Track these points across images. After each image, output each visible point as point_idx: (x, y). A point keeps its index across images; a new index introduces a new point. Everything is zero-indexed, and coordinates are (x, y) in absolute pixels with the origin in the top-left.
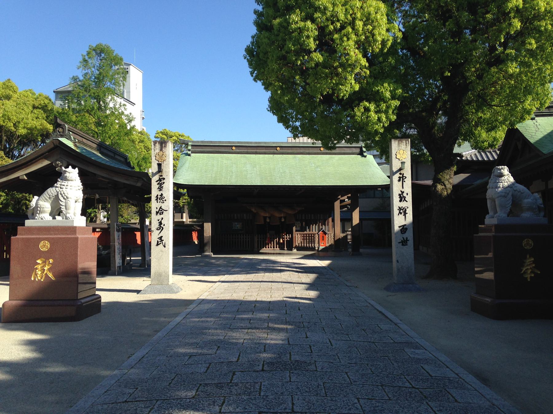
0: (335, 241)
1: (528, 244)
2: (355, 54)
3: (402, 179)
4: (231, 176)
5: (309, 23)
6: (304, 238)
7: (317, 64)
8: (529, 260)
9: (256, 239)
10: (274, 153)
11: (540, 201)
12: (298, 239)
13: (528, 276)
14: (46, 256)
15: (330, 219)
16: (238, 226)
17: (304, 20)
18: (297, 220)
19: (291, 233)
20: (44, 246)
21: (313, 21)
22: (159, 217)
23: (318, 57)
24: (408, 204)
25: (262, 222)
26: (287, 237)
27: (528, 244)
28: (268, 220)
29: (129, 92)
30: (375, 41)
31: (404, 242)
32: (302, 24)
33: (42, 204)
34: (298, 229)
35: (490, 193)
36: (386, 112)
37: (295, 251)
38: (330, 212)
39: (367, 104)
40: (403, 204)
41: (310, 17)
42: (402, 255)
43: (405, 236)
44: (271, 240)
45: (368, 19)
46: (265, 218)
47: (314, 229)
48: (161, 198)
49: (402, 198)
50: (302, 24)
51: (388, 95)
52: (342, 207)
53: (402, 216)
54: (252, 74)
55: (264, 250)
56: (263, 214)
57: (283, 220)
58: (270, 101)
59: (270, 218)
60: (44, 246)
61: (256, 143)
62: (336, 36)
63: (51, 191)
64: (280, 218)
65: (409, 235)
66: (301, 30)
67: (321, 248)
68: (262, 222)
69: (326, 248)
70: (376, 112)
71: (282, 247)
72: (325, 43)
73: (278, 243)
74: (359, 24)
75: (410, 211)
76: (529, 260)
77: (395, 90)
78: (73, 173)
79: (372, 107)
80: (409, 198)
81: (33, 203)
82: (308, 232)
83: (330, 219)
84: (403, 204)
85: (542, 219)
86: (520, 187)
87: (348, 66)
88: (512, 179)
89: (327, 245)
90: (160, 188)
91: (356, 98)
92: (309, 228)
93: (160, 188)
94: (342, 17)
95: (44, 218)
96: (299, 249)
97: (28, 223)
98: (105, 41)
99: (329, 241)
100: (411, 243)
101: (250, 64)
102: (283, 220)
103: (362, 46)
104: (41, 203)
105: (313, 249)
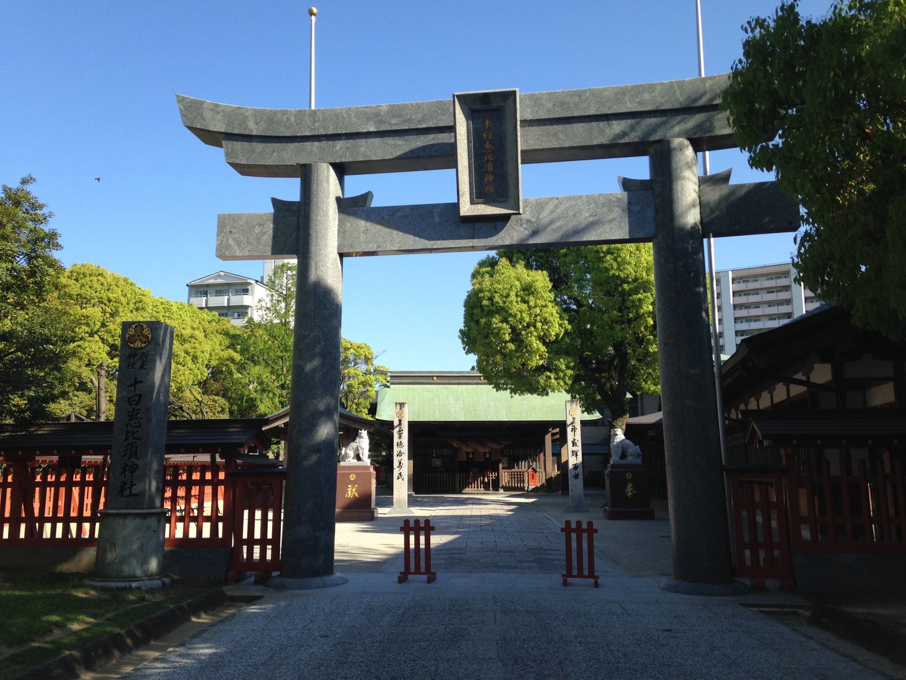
0: (547, 480)
1: (629, 476)
2: (537, 344)
4: (434, 411)
5: (505, 324)
6: (512, 476)
7: (511, 351)
8: (630, 485)
9: (458, 479)
10: (478, 384)
11: (639, 450)
12: (505, 477)
13: (629, 495)
14: (353, 483)
15: (542, 454)
16: (437, 462)
17: (502, 322)
20: (353, 477)
21: (507, 322)
22: (399, 458)
23: (512, 346)
24: (579, 449)
25: (465, 458)
26: (493, 476)
27: (629, 476)
28: (471, 456)
30: (550, 335)
31: (576, 476)
32: (500, 325)
33: (349, 451)
34: (505, 466)
35: (611, 446)
36: (564, 378)
37: (502, 491)
38: (541, 447)
39: (548, 374)
40: (575, 449)
41: (505, 320)
42: (576, 486)
43: (577, 472)
44: (475, 479)
45: (545, 322)
46: (468, 453)
47: (523, 466)
48: (400, 444)
49: (574, 444)
50: (500, 325)
51: (563, 367)
52: (553, 441)
53: (574, 457)
54: (464, 348)
55: (467, 490)
57: (488, 456)
58: (465, 306)
59: (473, 453)
60: (353, 477)
61: (459, 372)
62: (523, 332)
63: (353, 445)
64: (485, 454)
65: (580, 471)
66: (500, 329)
67: (531, 487)
68: (465, 458)
69: (537, 487)
70: (555, 379)
71: (486, 487)
72: (516, 337)
73: (483, 482)
74: (539, 325)
75: (580, 454)
76: (630, 485)
77: (569, 363)
78: (364, 433)
79: (552, 376)
80: (579, 444)
81: (343, 452)
82: (516, 469)
83: (542, 454)
84: (575, 449)
85: (639, 461)
86: (628, 441)
87: (531, 352)
88: (623, 437)
89: (539, 485)
90: (400, 437)
91: (540, 369)
92: (518, 465)
93: (400, 437)
94: (527, 319)
95: (351, 461)
96: (506, 489)
97: (342, 464)
99: (539, 480)
100: (581, 477)
101: (463, 342)
102: (488, 456)
103: (542, 339)
104: (348, 452)
105: (522, 489)
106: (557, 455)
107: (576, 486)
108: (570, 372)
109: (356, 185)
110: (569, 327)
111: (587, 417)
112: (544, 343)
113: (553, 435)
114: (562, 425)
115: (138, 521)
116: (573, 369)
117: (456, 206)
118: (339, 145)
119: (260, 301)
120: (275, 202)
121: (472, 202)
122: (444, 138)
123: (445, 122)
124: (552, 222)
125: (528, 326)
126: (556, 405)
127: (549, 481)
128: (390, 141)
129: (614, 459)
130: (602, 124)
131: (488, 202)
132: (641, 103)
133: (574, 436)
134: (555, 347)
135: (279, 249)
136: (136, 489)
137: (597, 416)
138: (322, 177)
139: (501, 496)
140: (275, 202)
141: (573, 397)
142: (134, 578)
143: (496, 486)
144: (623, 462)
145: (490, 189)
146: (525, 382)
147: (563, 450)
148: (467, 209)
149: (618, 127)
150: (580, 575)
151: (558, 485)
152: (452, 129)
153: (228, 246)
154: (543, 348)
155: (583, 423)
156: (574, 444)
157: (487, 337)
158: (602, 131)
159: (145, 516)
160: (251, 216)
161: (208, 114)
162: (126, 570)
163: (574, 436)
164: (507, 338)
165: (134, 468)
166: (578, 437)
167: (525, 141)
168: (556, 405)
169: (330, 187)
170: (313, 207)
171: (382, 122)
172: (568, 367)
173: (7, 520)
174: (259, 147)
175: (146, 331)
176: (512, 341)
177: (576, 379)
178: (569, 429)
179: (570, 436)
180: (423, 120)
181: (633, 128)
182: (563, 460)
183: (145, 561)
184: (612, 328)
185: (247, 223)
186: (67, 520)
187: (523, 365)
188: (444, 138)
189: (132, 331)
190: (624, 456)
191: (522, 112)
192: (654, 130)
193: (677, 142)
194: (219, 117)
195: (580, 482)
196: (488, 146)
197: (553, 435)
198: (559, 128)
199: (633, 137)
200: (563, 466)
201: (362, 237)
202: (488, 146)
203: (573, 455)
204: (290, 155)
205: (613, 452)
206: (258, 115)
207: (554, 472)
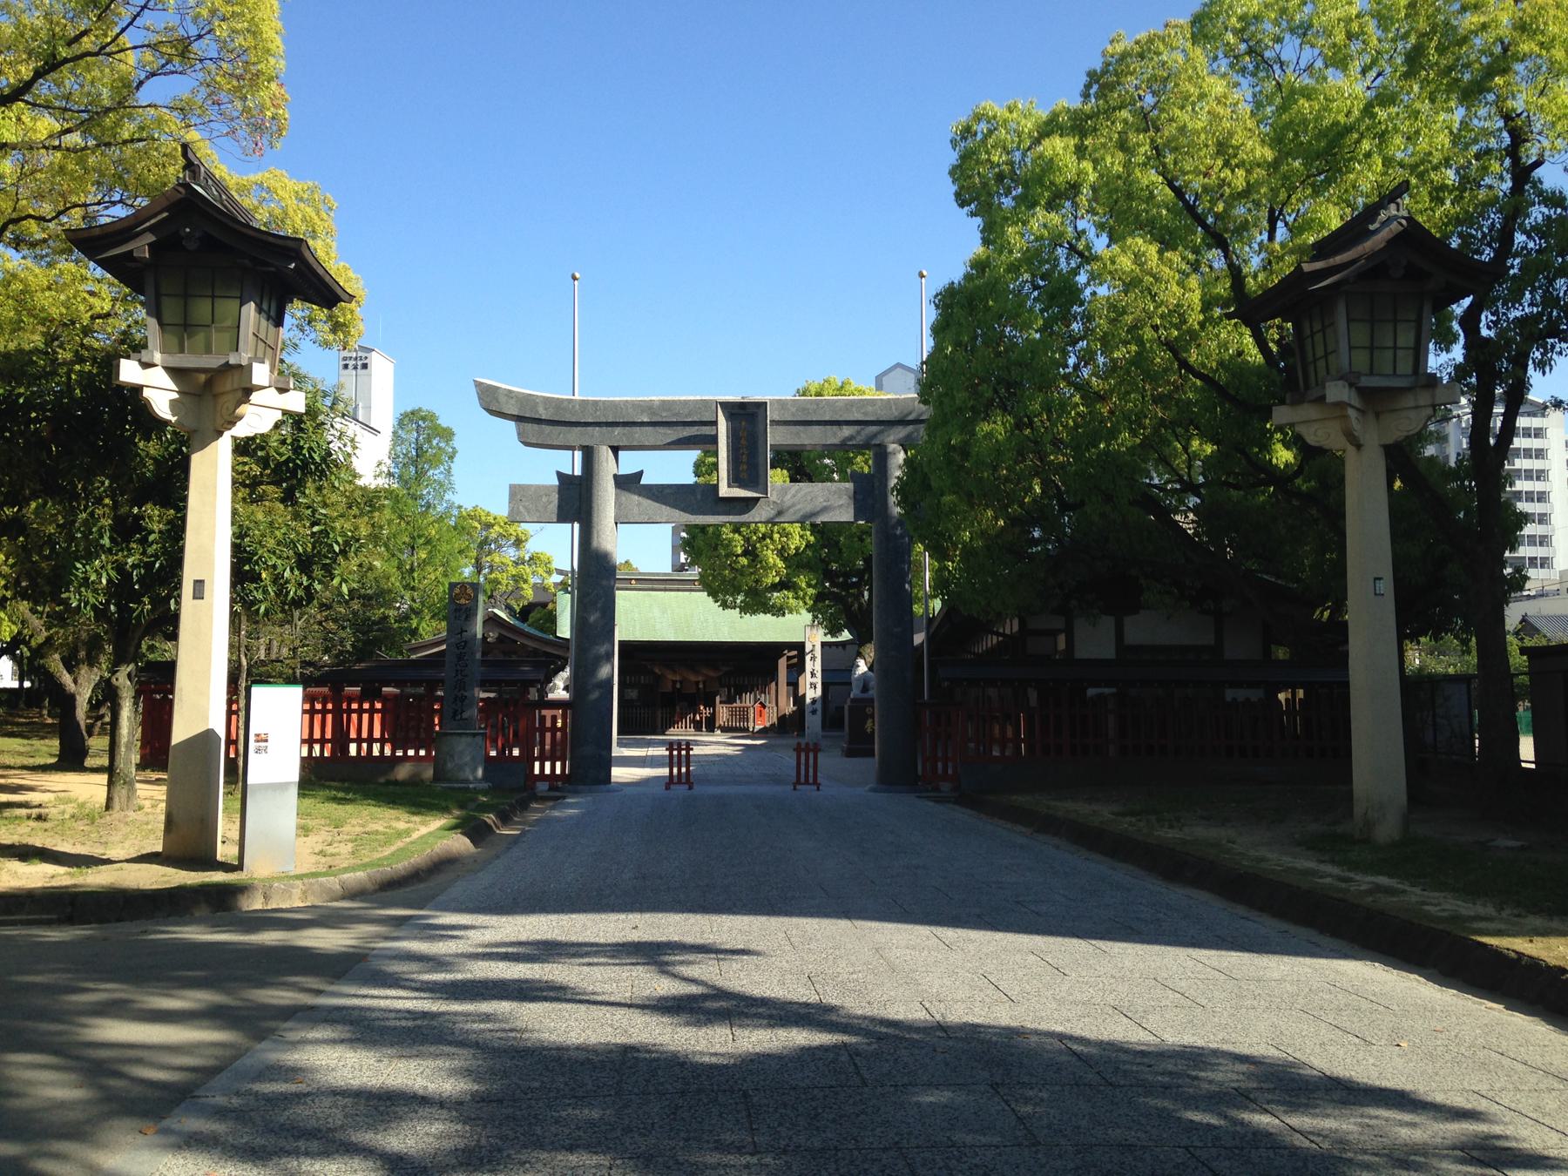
2: (772, 558)
3: (813, 659)
6: (732, 713)
12: (723, 713)
18: (722, 686)
19: (711, 703)
23: (744, 561)
24: (818, 680)
29: (368, 408)
31: (814, 712)
38: (773, 676)
42: (813, 723)
44: (683, 716)
46: (674, 682)
47: (748, 700)
49: (813, 675)
56: (671, 677)
65: (819, 706)
66: (730, 541)
67: (758, 728)
71: (698, 727)
73: (693, 721)
74: (776, 536)
75: (819, 686)
80: (819, 675)
82: (738, 704)
87: (767, 568)
96: (724, 730)
98: (427, 406)
99: (769, 718)
100: (819, 712)
103: (781, 553)
105: (747, 730)
106: (793, 684)
107: (813, 723)
108: (811, 591)
109: (630, 462)
110: (812, 539)
111: (829, 639)
112: (784, 559)
113: (789, 658)
114: (800, 647)
115: (469, 739)
116: (814, 587)
117: (716, 487)
118: (617, 431)
119: (380, 464)
120: (560, 475)
121: (729, 486)
122: (707, 430)
123: (707, 417)
124: (793, 505)
125: (764, 538)
126: (796, 625)
127: (782, 719)
128: (661, 430)
129: (855, 692)
130: (835, 428)
131: (742, 486)
132: (865, 414)
133: (813, 665)
134: (796, 562)
135: (562, 518)
136: (465, 715)
137: (846, 635)
138: (603, 458)
139: (718, 736)
140: (560, 475)
141: (815, 617)
142: (467, 781)
143: (711, 726)
144: (865, 696)
145: (744, 475)
146: (757, 602)
147: (801, 679)
148: (724, 491)
149: (847, 431)
150: (807, 782)
151: (788, 726)
152: (715, 423)
153: (519, 512)
154: (780, 564)
155: (823, 644)
156: (813, 675)
157: (715, 549)
158: (835, 434)
159: (474, 735)
160: (538, 487)
161: (502, 399)
162: (462, 776)
163: (813, 665)
164: (739, 551)
165: (463, 699)
166: (818, 667)
167: (773, 437)
168: (796, 625)
169: (608, 468)
170: (596, 478)
171: (654, 414)
172: (809, 585)
173: (353, 741)
174: (547, 429)
175: (469, 591)
176: (745, 553)
177: (819, 598)
178: (808, 658)
179: (809, 665)
180: (689, 415)
181: (858, 433)
182: (801, 693)
183: (474, 770)
184: (862, 540)
185: (537, 492)
186: (359, 741)
187: (757, 581)
188: (707, 430)
189: (457, 591)
190: (865, 689)
191: (771, 415)
192: (875, 435)
193: (892, 447)
194: (513, 402)
195: (818, 718)
196: (743, 442)
197: (789, 658)
198: (801, 428)
199: (859, 440)
200: (799, 700)
201: (636, 510)
202: (743, 442)
203: (811, 687)
204: (574, 435)
205: (854, 685)
206: (548, 401)
207: (789, 707)
